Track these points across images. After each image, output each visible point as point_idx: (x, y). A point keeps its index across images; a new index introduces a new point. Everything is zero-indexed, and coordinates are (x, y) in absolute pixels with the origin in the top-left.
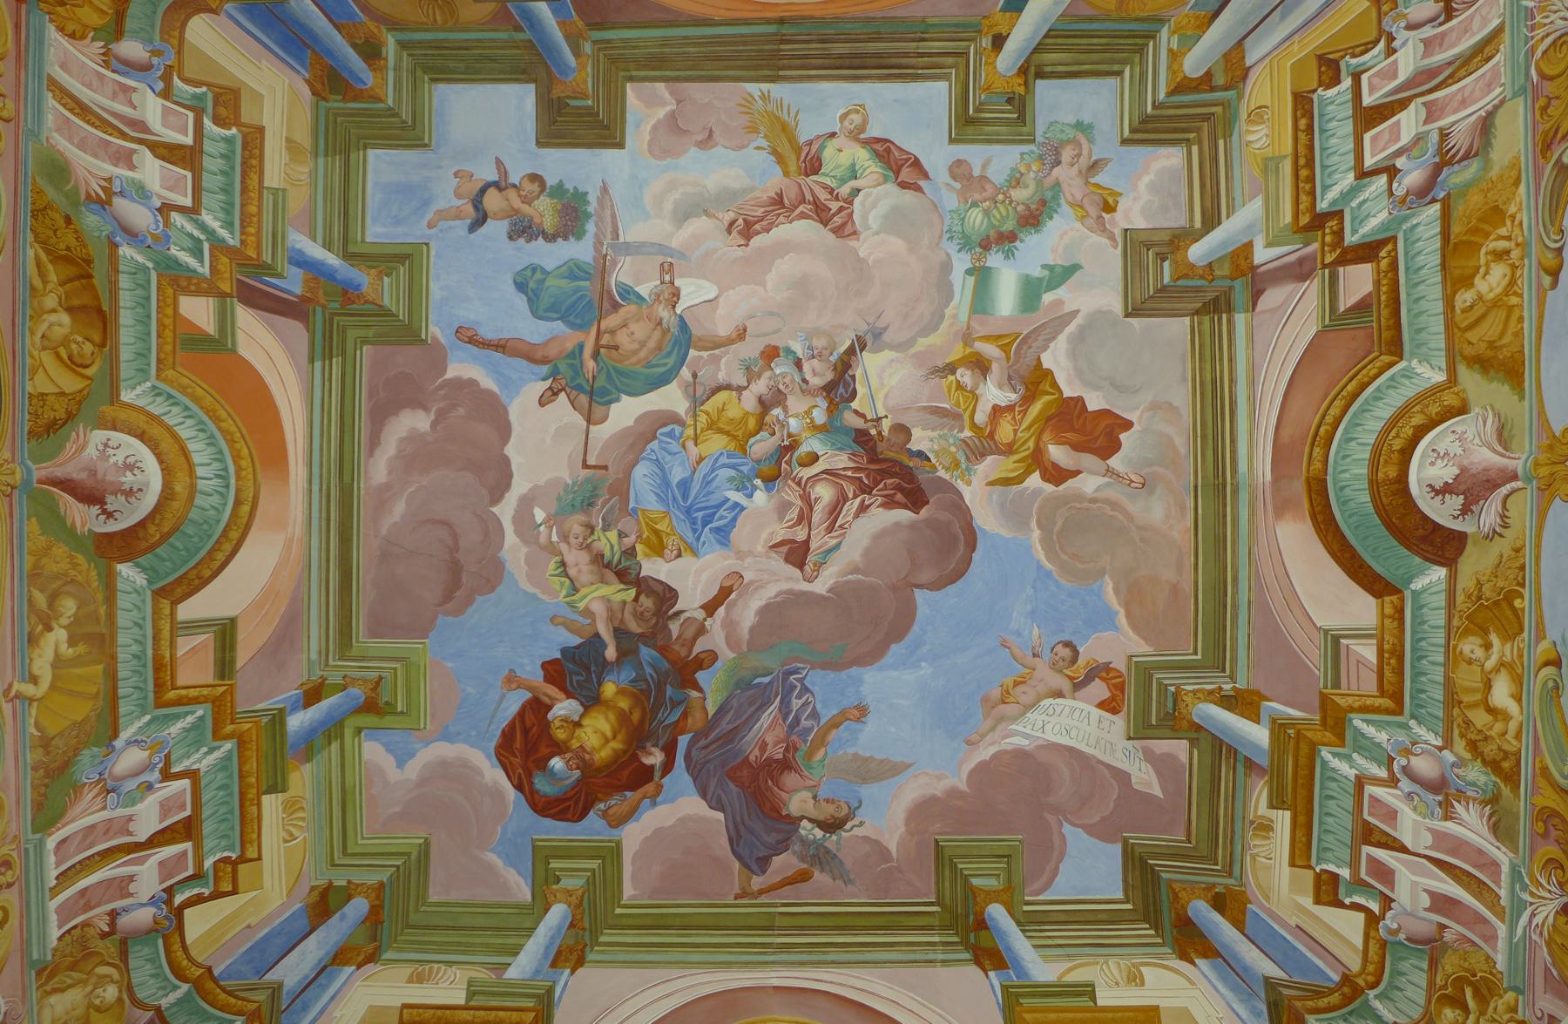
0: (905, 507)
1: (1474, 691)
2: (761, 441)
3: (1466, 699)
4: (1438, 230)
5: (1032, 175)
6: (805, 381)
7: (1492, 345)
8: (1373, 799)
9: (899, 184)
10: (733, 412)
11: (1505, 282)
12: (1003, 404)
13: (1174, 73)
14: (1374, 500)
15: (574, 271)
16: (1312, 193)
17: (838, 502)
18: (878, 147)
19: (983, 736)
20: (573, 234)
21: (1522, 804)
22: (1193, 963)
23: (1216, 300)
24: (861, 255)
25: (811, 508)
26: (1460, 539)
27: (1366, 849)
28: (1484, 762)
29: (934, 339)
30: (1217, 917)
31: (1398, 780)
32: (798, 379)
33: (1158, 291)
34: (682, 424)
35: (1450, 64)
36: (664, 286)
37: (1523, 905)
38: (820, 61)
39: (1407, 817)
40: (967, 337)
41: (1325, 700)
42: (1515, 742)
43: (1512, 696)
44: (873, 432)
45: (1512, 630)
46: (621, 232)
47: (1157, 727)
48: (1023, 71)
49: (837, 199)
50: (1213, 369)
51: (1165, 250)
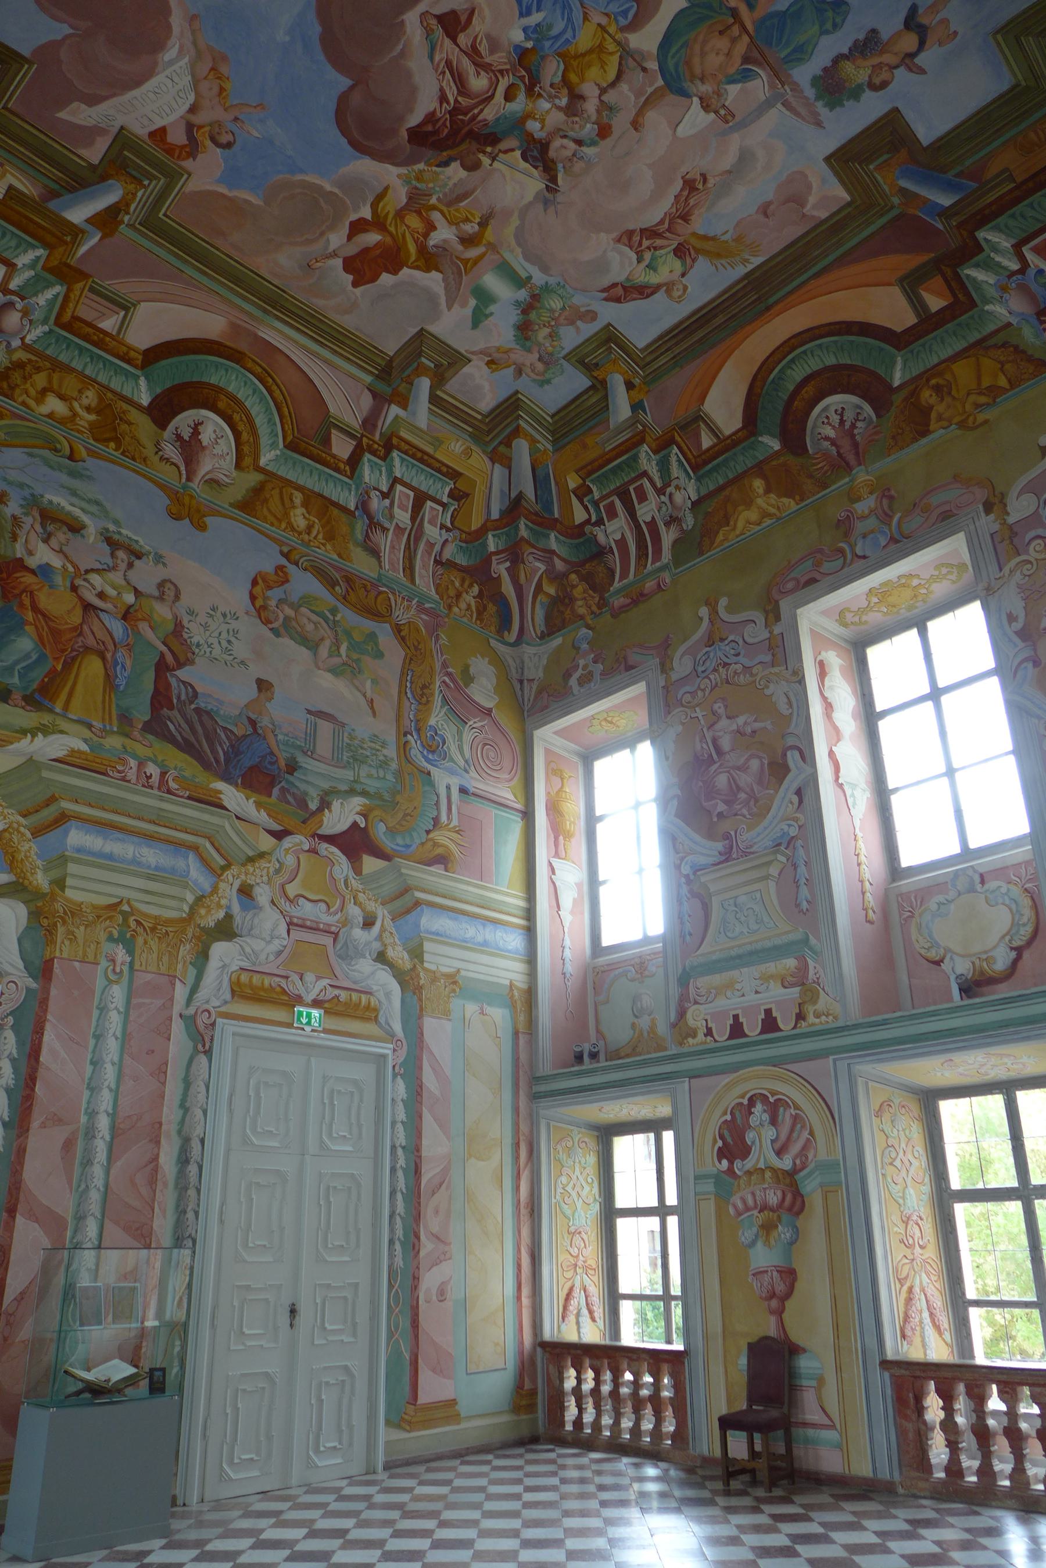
0: (418, 126)
2: (556, 73)
3: (56, 377)
5: (547, 345)
6: (565, 137)
7: (266, 501)
9: (617, 284)
10: (594, 72)
11: (295, 526)
12: (432, 234)
14: (209, 384)
15: (801, 53)
16: (406, 453)
17: (463, 86)
18: (649, 291)
19: (193, 32)
20: (821, 77)
24: (602, 234)
25: (475, 64)
26: (163, 426)
28: (8, 368)
29: (510, 231)
31: (4, 295)
32: (571, 134)
34: (623, 29)
35: (415, 551)
36: (719, 105)
38: (727, 304)
40: (492, 247)
41: (84, 275)
42: (20, 400)
44: (489, 149)
46: (783, 109)
48: (603, 383)
49: (649, 248)
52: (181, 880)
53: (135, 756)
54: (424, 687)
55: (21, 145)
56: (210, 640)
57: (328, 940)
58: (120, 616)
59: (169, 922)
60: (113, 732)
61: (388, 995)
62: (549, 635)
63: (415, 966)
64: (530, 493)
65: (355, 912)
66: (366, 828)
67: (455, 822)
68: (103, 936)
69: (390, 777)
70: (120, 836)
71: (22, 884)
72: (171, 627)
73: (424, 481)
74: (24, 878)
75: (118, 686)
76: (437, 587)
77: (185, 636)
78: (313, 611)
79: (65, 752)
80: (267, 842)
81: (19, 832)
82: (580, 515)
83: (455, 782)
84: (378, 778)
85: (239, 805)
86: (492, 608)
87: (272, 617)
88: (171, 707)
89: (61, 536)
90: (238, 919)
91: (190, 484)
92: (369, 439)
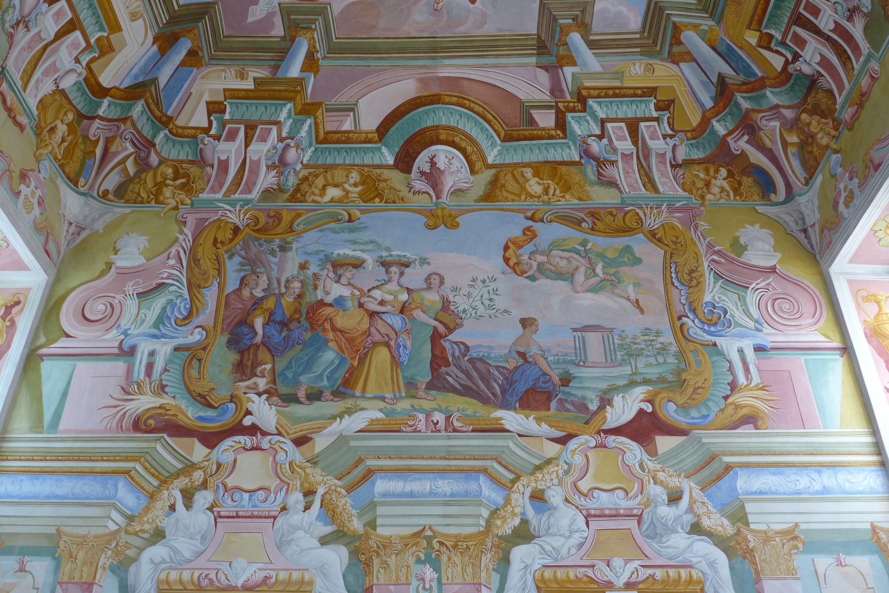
1: (333, 179)
3: (329, 175)
4: (566, 160)
7: (503, 186)
8: (270, 130)
11: (533, 193)
13: (686, 26)
14: (428, 128)
16: (599, 96)
21: (280, 204)
22: (153, 44)
23: (545, 47)
26: (408, 171)
27: (242, 127)
28: (299, 184)
30: (184, 53)
31: (282, 142)
33: (554, 16)
35: (649, 166)
37: (234, 206)
39: (265, 147)
42: (310, 200)
43: (332, 198)
45: (366, 197)
47: (290, 20)
50: (504, 46)
51: (579, 20)
52: (476, 499)
53: (421, 411)
54: (692, 271)
55: (244, 52)
56: (474, 305)
57: (632, 524)
58: (398, 312)
59: (468, 537)
60: (401, 398)
61: (712, 565)
62: (811, 178)
63: (739, 530)
64: (727, 70)
65: (658, 492)
66: (653, 413)
67: (756, 380)
68: (411, 560)
69: (671, 360)
70: (418, 476)
71: (342, 531)
72: (440, 305)
73: (628, 110)
74: (343, 526)
75: (402, 363)
76: (683, 187)
77: (452, 308)
78: (563, 250)
79: (366, 423)
80: (552, 449)
81: (336, 491)
82: (778, 63)
83: (748, 345)
84: (659, 364)
85: (520, 424)
86: (747, 181)
87: (526, 268)
88: (448, 364)
89: (348, 273)
90: (534, 522)
91: (440, 200)
92: (562, 102)
